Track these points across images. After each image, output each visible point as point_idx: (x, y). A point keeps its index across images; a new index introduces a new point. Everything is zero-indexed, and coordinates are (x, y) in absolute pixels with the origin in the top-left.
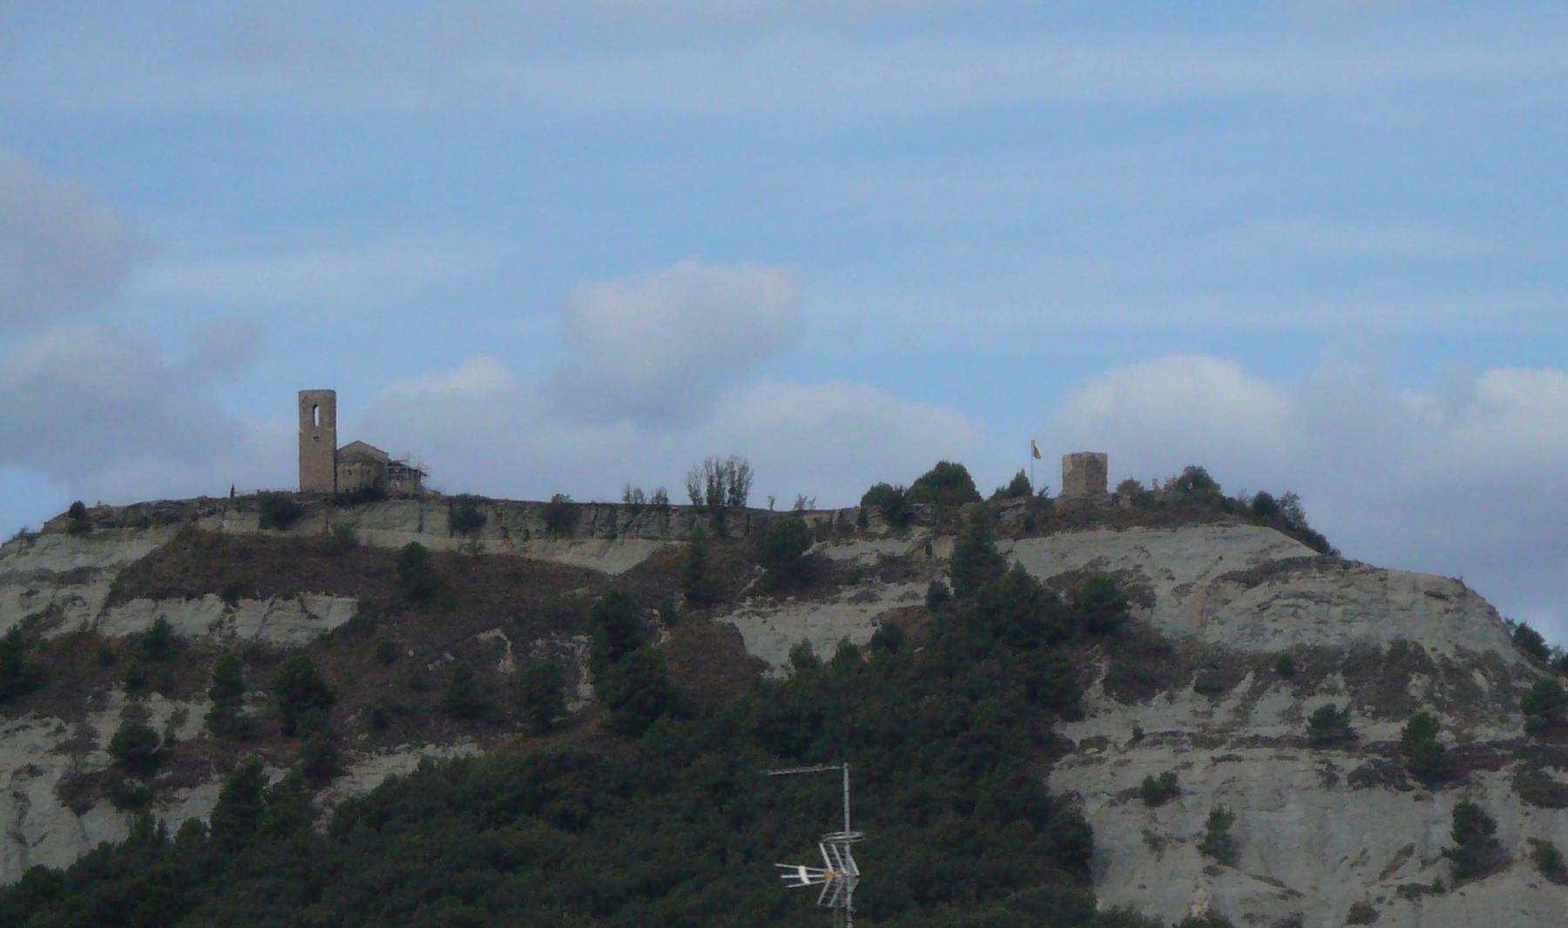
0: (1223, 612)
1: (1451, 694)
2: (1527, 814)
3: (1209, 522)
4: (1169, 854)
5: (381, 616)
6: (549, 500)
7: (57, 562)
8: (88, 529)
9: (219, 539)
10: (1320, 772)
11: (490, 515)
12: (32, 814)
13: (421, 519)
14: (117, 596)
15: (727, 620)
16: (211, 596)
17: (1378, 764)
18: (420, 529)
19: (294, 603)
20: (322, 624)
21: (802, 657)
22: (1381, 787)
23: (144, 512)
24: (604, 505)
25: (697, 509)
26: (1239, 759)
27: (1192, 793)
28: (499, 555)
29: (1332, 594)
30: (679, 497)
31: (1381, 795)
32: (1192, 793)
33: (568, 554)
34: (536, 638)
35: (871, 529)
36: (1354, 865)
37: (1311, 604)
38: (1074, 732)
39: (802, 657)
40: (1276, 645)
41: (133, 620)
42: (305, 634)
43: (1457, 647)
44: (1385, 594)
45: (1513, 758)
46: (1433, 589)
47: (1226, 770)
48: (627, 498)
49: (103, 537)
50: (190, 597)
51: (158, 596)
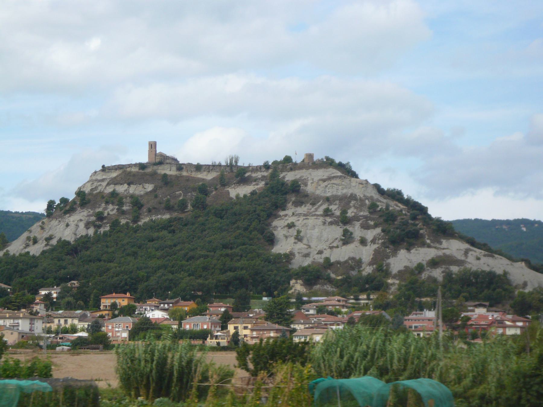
0: (319, 188)
1: (359, 205)
2: (361, 231)
3: (325, 168)
4: (289, 239)
5: (158, 189)
6: (196, 164)
7: (99, 177)
8: (105, 170)
9: (130, 172)
10: (323, 222)
11: (184, 167)
12: (79, 229)
13: (171, 168)
14: (108, 184)
15: (228, 189)
16: (126, 184)
17: (334, 220)
18: (170, 170)
19: (141, 186)
20: (147, 190)
21: (237, 196)
22: (334, 225)
23: (116, 167)
24: (208, 165)
25: (227, 166)
26: (308, 219)
27: (298, 226)
28: (186, 176)
29: (339, 183)
30: (223, 163)
31: (334, 227)
32: (298, 226)
33: (200, 175)
34: (189, 193)
35: (262, 170)
36: (325, 242)
37: (336, 186)
38: (282, 213)
39: (237, 196)
40: (328, 195)
41: (110, 189)
42: (143, 192)
43: (364, 195)
44: (350, 183)
45: (363, 219)
46: (360, 182)
47: (305, 221)
48: (213, 163)
49: (108, 172)
50: (121, 184)
51: (115, 184)
